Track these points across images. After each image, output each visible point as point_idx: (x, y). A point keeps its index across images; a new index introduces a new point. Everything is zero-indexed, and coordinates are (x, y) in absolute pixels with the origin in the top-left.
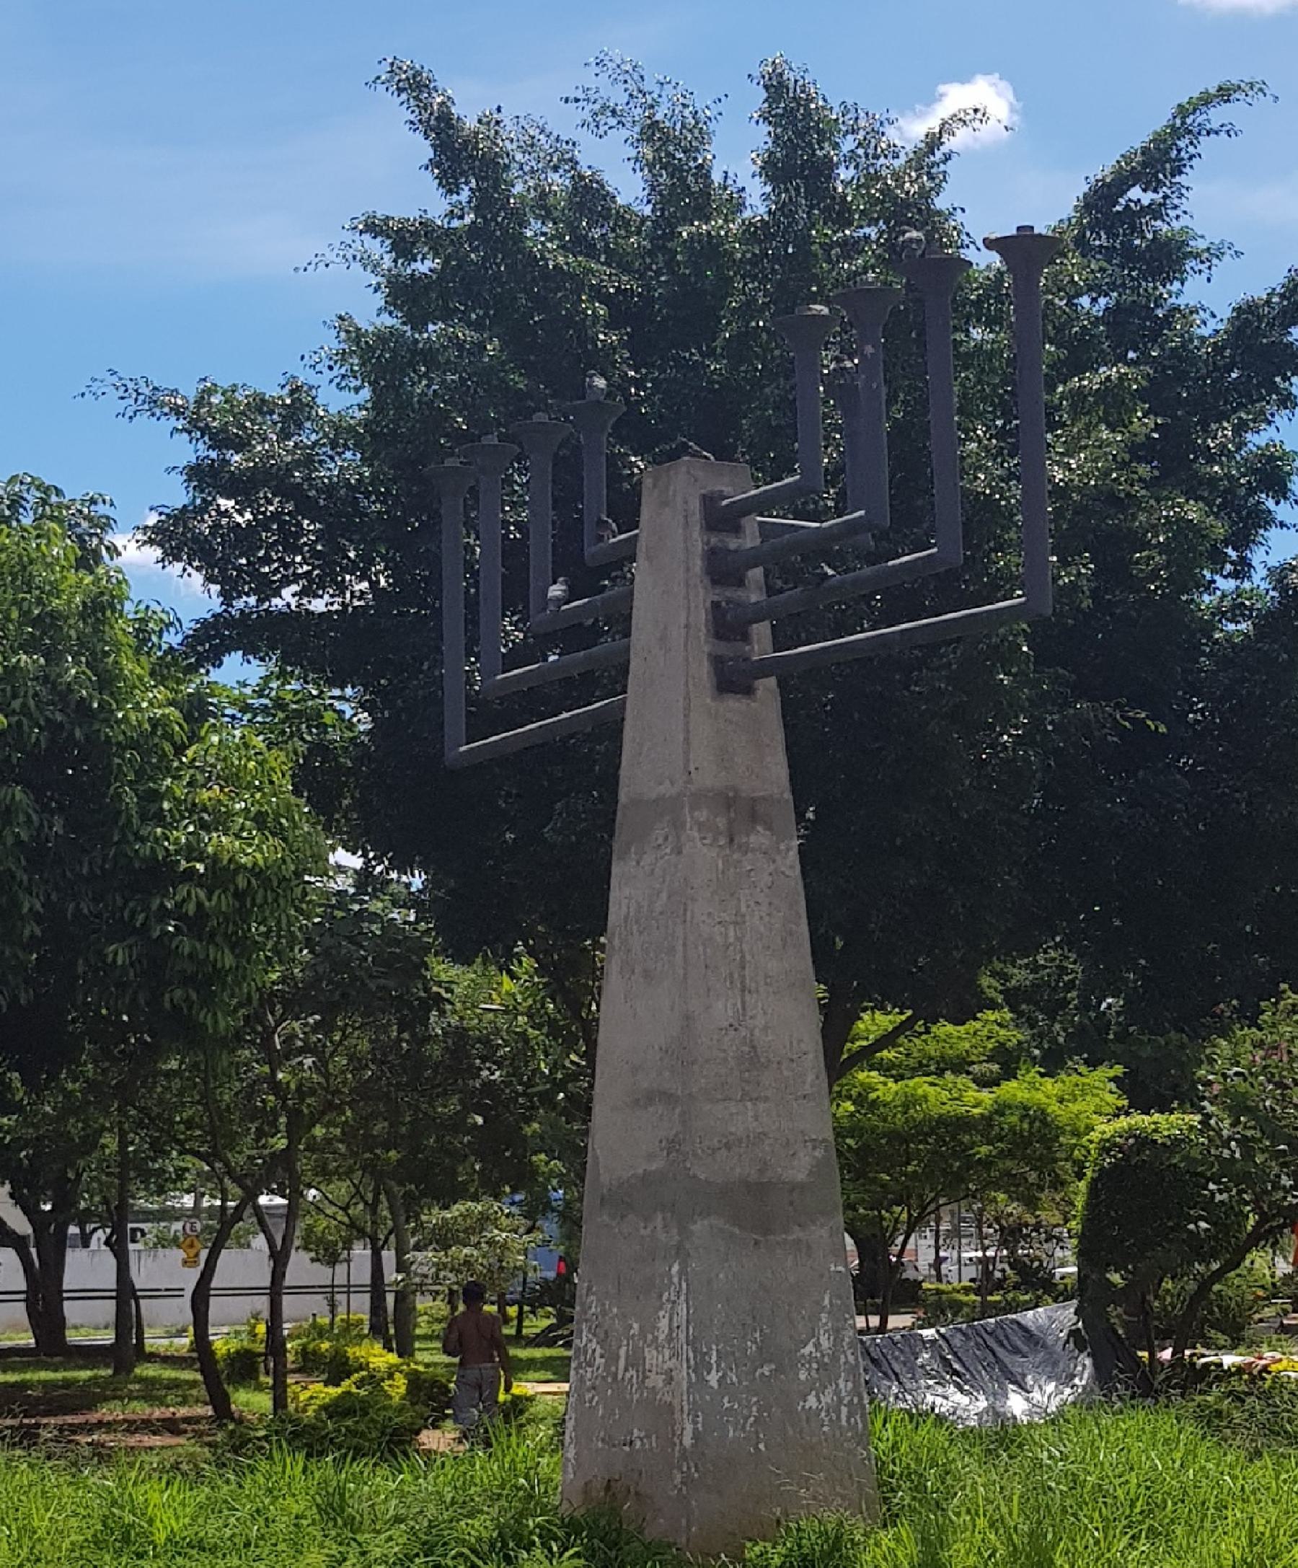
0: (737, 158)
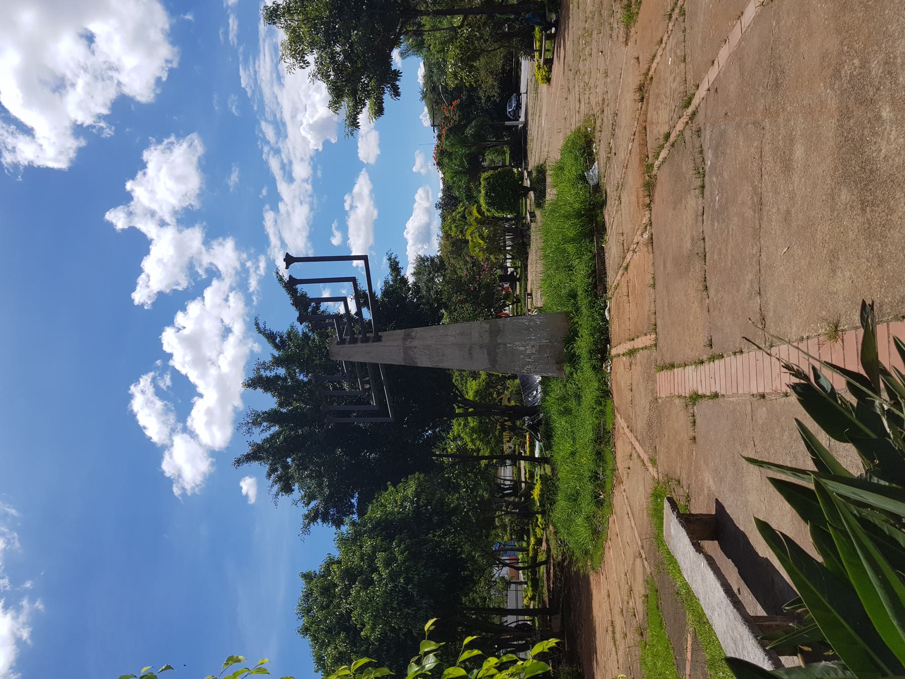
0: (268, 402)
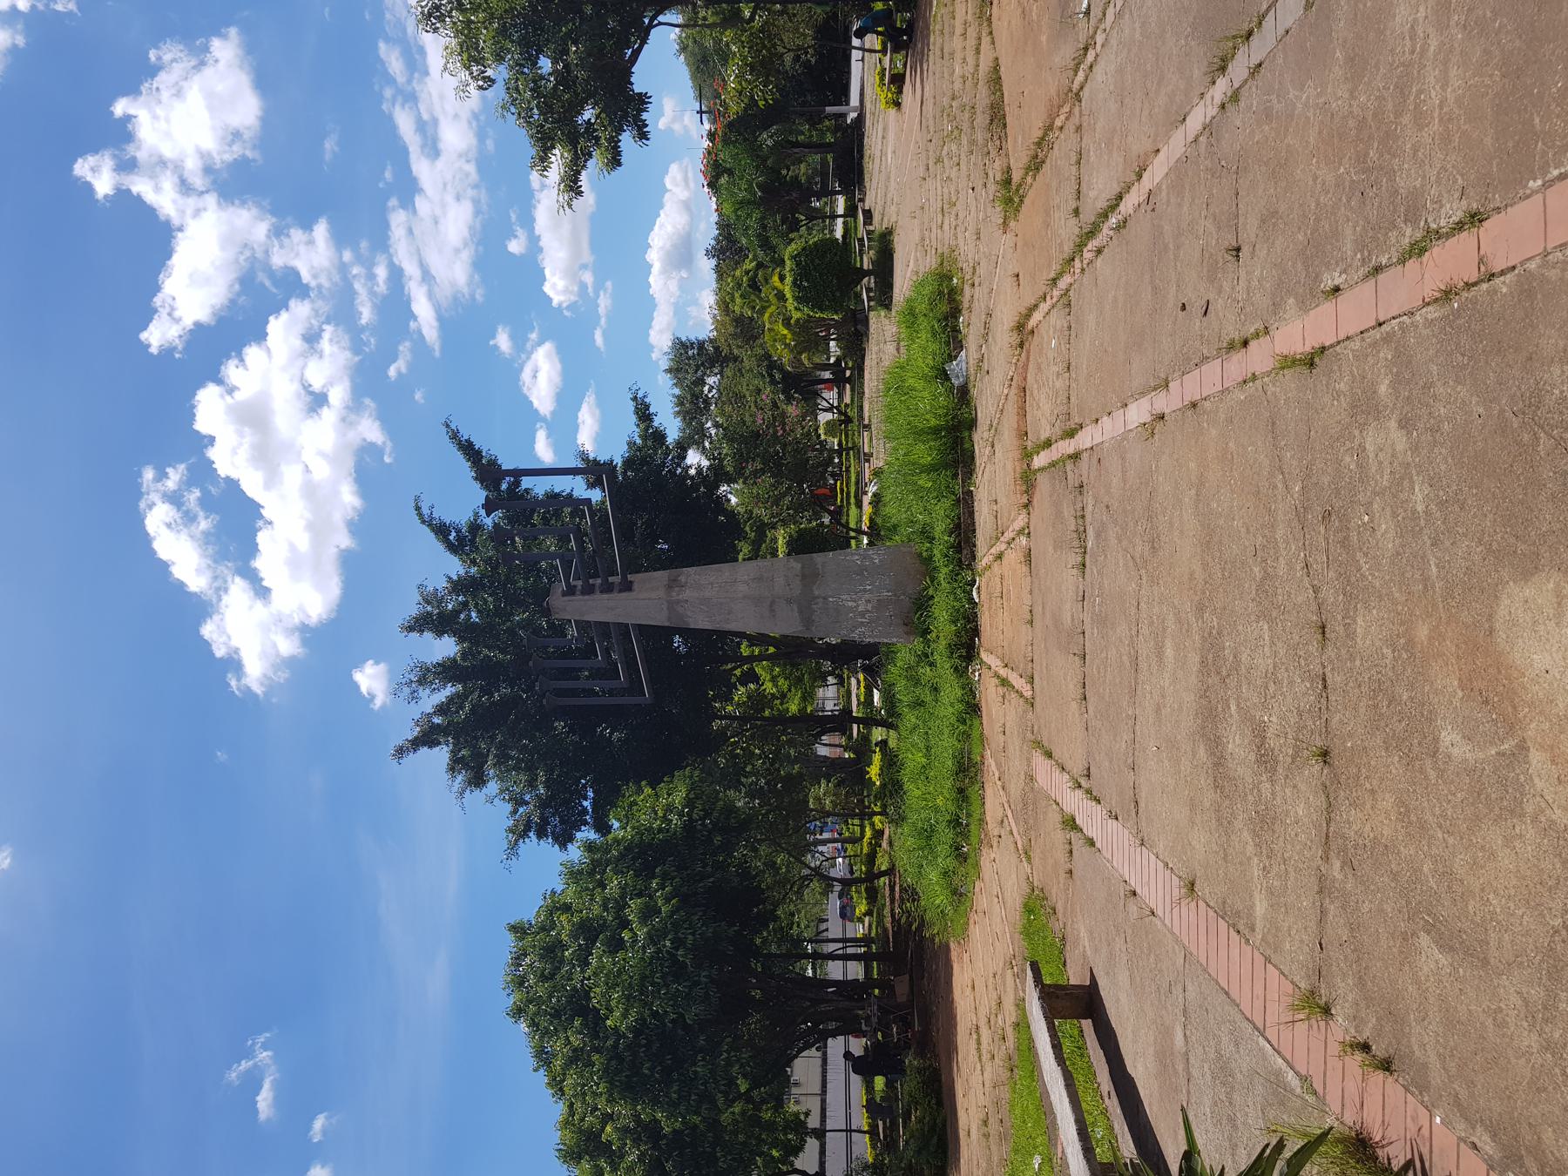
0: (445, 648)
